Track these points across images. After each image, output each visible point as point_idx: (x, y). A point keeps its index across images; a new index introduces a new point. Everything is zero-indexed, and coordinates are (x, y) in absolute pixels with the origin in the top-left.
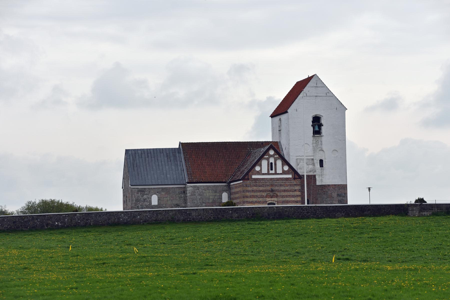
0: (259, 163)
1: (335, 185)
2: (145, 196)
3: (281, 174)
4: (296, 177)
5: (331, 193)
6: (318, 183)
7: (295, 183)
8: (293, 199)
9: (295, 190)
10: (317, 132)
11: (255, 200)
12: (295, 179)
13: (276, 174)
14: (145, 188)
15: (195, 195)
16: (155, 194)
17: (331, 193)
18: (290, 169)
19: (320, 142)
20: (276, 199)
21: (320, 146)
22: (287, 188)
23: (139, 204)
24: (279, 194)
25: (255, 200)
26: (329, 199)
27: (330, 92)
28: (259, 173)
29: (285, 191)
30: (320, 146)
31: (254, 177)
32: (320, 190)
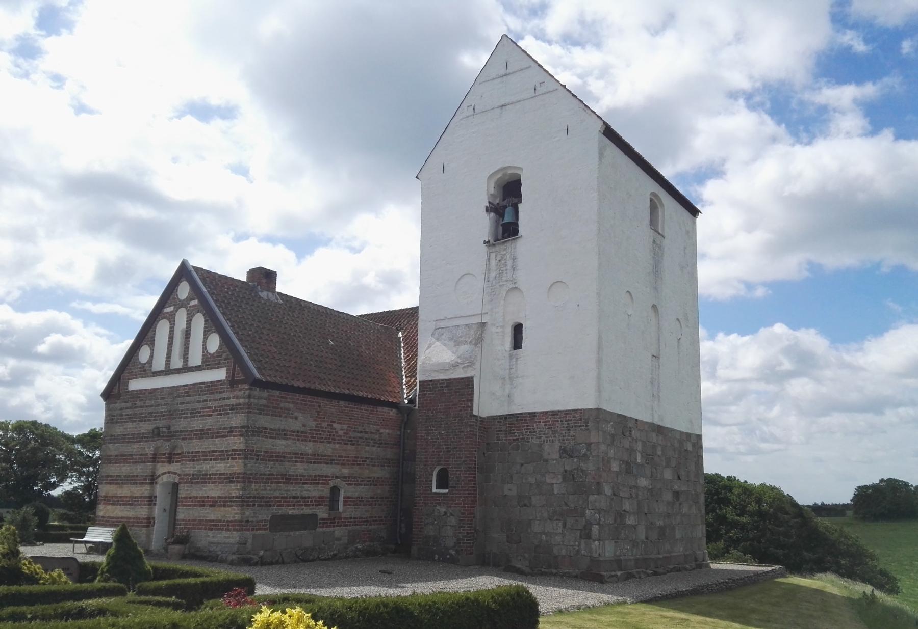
1: (554, 413)
3: (198, 368)
5: (540, 445)
7: (233, 401)
9: (231, 432)
10: (506, 229)
17: (540, 445)
19: (509, 263)
22: (209, 423)
24: (185, 447)
29: (203, 434)
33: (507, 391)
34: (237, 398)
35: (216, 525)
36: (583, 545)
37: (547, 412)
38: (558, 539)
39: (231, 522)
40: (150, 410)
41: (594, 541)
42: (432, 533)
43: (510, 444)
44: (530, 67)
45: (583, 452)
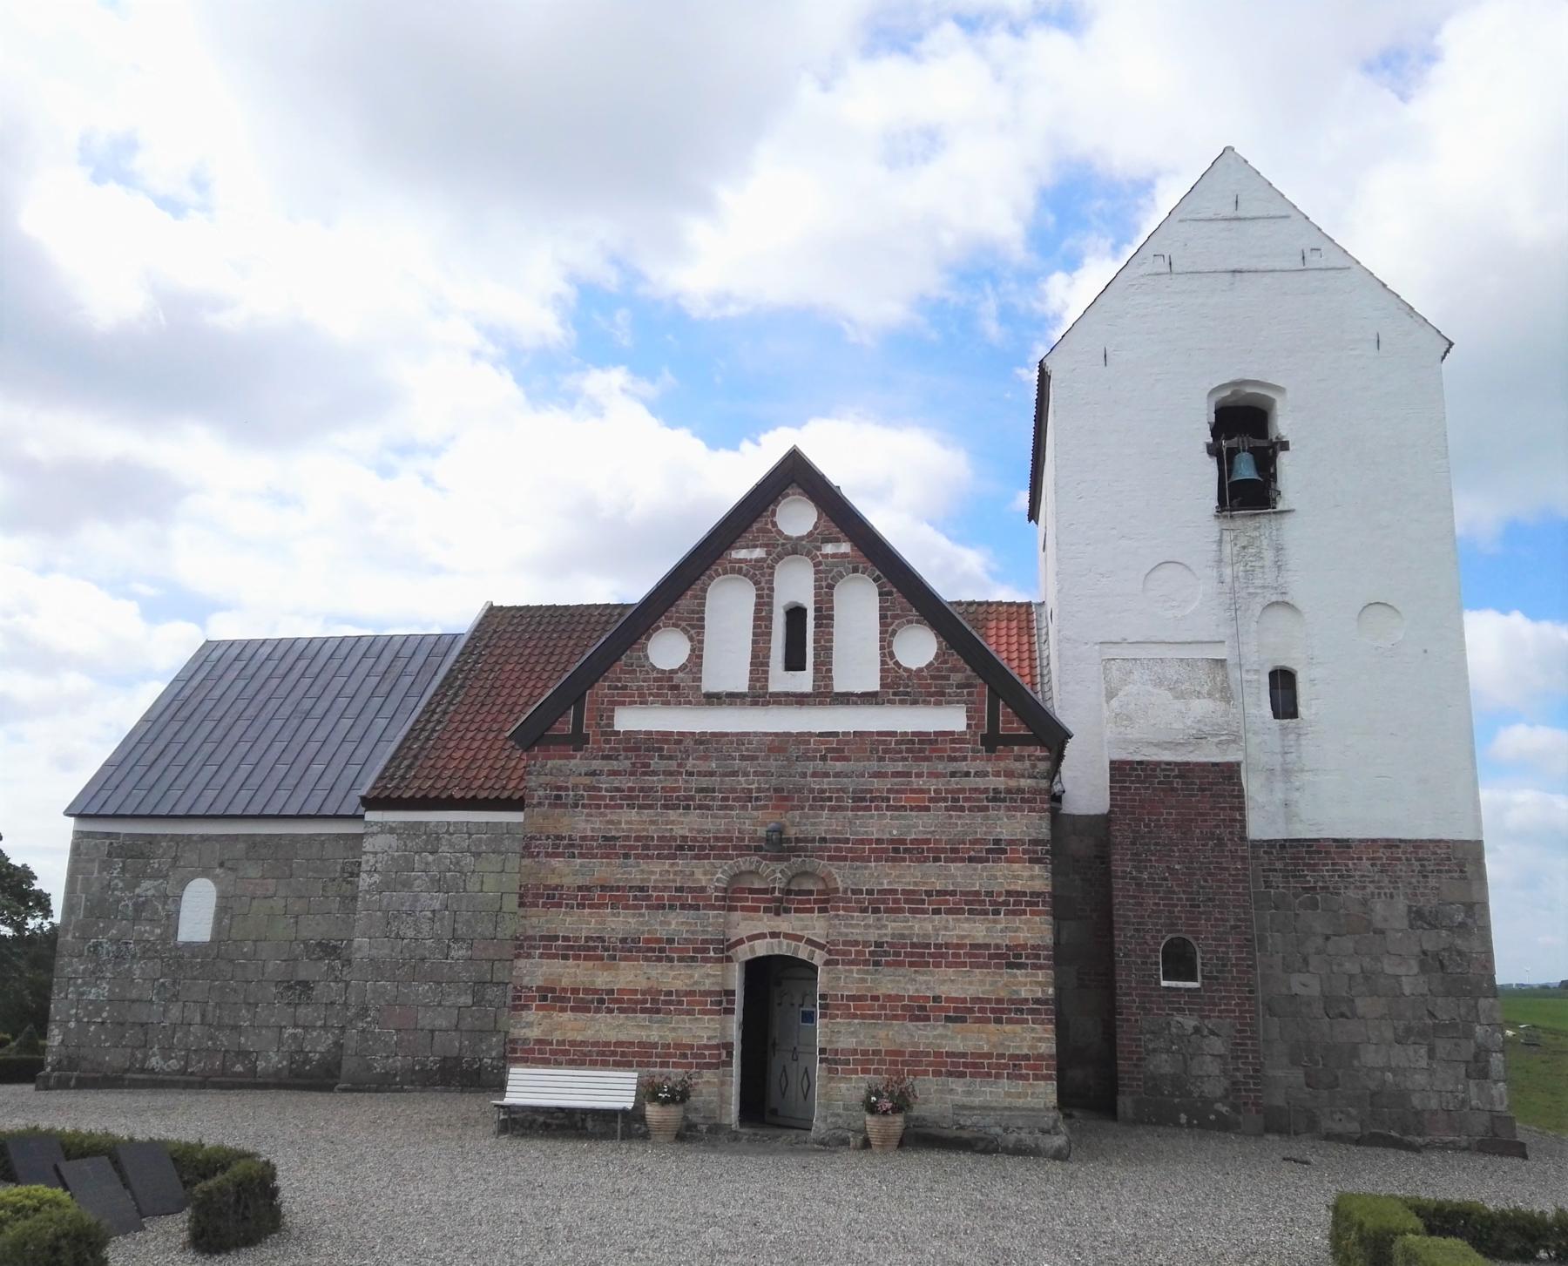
0: (685, 603)
1: (1391, 844)
2: (146, 884)
3: (868, 698)
4: (1010, 724)
5: (1364, 903)
6: (1260, 826)
7: (1001, 783)
8: (976, 930)
9: (998, 850)
11: (619, 923)
12: (992, 741)
13: (825, 696)
14: (151, 839)
15: (407, 884)
16: (205, 873)
17: (1364, 903)
18: (955, 659)
19: (1269, 555)
20: (815, 926)
21: (1270, 577)
22: (919, 825)
23: (104, 931)
24: (842, 877)
25: (619, 923)
26: (1348, 944)
27: (1325, 246)
28: (678, 688)
29: (896, 850)
30: (1270, 577)
31: (629, 720)
32: (1277, 879)
33: (1279, 796)
34: (1009, 774)
35: (974, 1065)
36: (1473, 1090)
37: (1374, 841)
38: (1421, 1079)
39: (1026, 1057)
40: (705, 782)
41: (1496, 1082)
42: (1167, 1069)
43: (1296, 896)
44: (1287, 217)
45: (1460, 918)
